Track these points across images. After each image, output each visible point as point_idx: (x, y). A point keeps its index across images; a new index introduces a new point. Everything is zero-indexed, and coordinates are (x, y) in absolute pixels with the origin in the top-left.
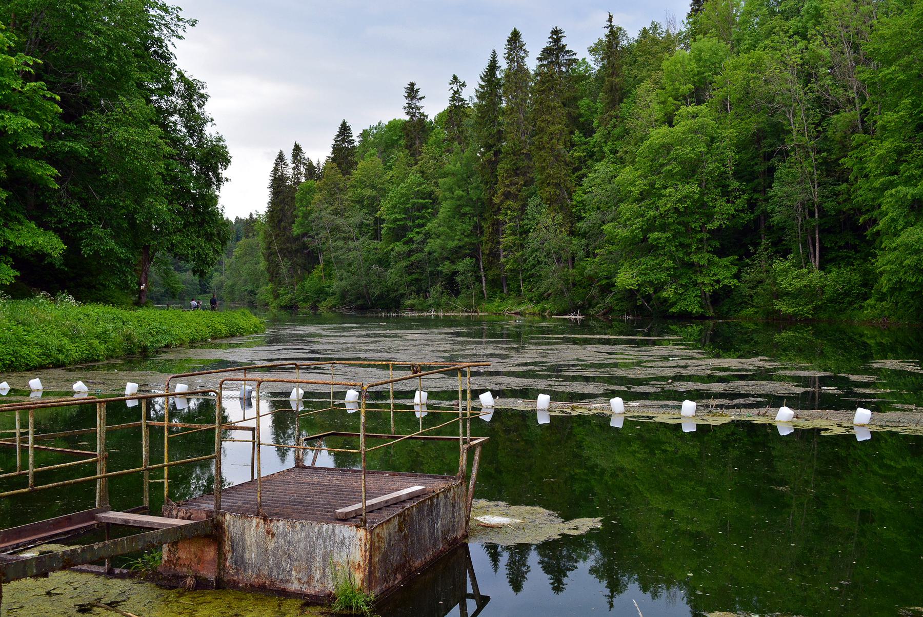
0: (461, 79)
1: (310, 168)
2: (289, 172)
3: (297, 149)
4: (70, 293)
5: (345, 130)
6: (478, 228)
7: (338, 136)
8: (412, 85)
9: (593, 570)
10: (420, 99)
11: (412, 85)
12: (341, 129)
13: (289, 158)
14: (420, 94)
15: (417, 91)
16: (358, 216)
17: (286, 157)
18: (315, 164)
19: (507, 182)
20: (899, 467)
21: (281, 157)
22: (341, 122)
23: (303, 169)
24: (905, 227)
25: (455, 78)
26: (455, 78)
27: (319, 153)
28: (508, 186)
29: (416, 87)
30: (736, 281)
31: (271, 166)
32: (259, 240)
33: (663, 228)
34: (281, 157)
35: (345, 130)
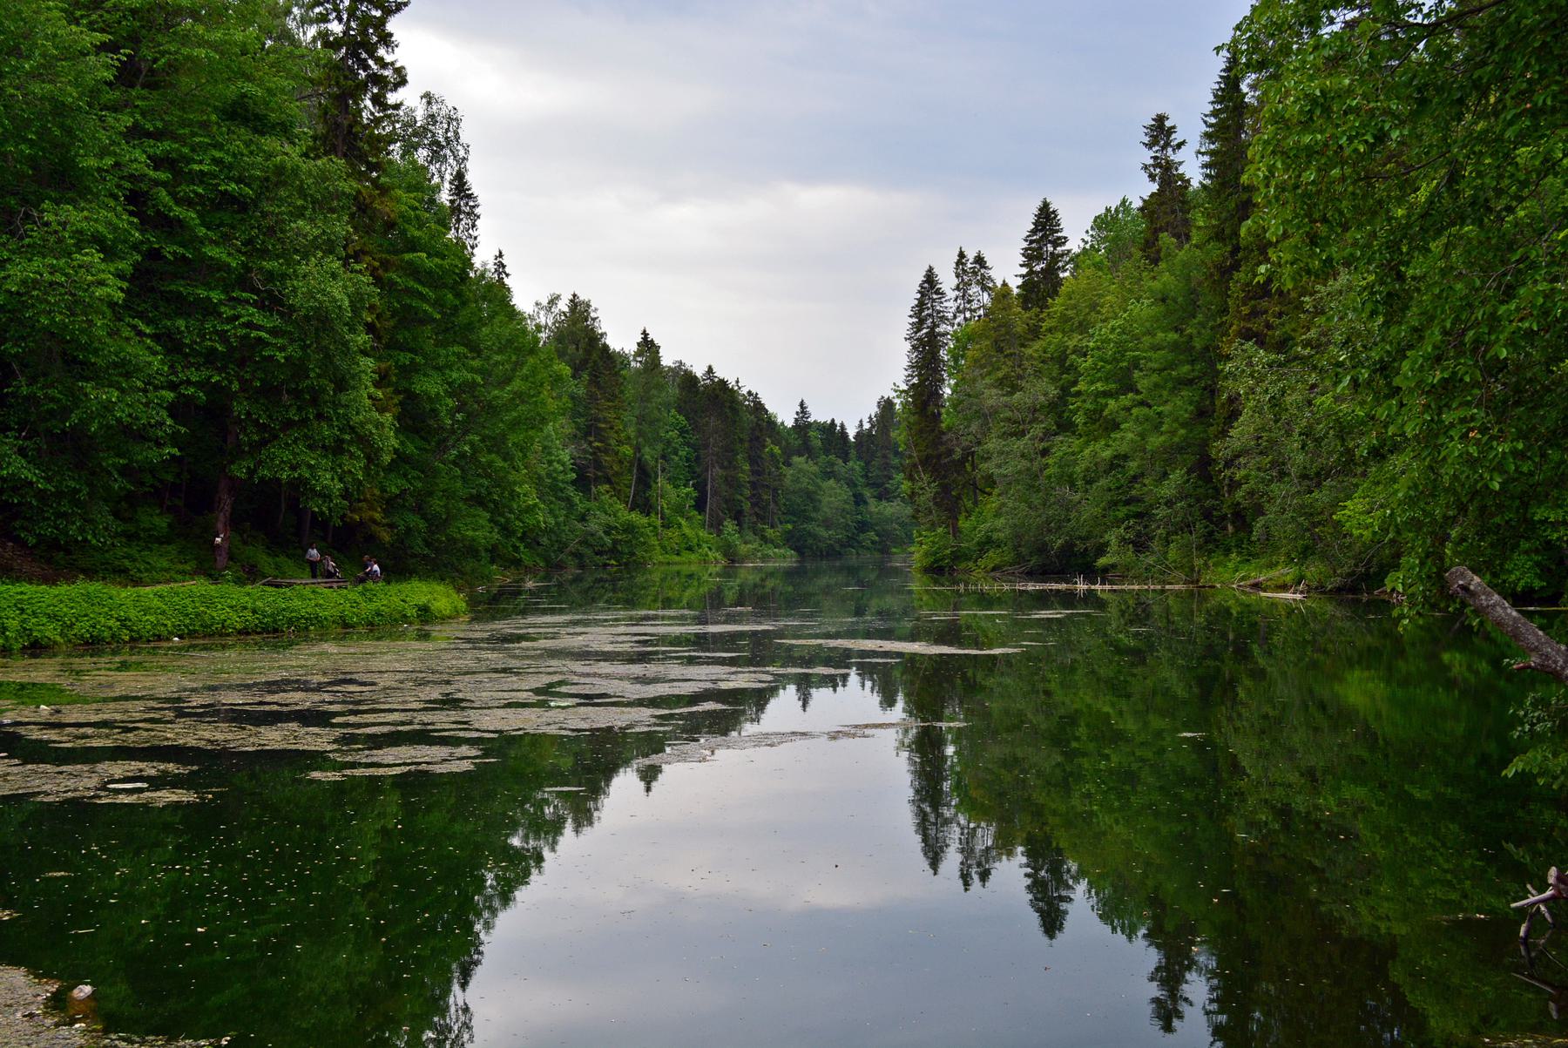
4: (513, 314)
6: (302, 193)
7: (1033, 232)
8: (1160, 119)
9: (1145, 936)
10: (1179, 146)
11: (1160, 119)
12: (1038, 216)
13: (948, 281)
14: (1177, 138)
15: (1172, 130)
16: (1041, 390)
17: (940, 278)
19: (1245, 310)
21: (930, 280)
22: (1039, 204)
28: (1248, 318)
29: (1168, 124)
30: (1130, 395)
34: (930, 280)
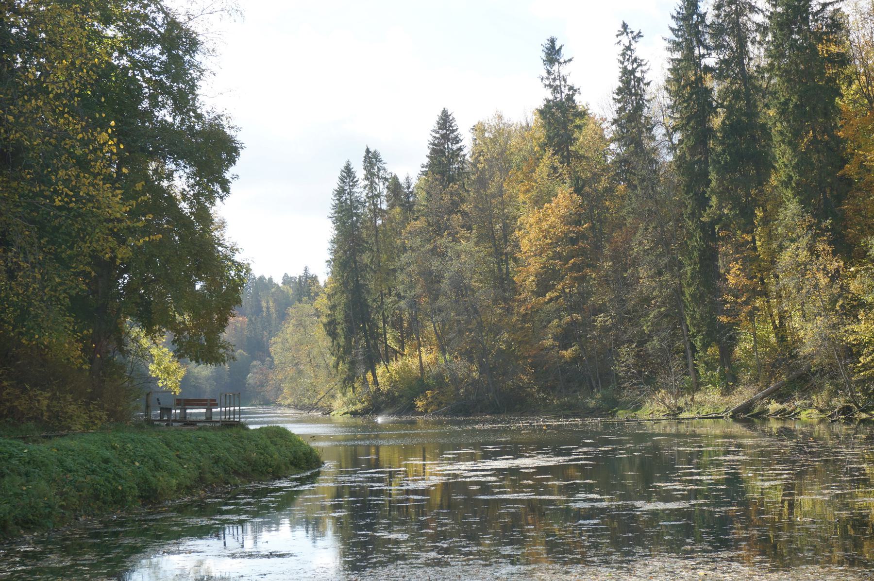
0: (633, 27)
1: (395, 187)
2: (361, 191)
3: (371, 159)
5: (445, 121)
11: (553, 41)
13: (360, 173)
14: (565, 55)
18: (402, 180)
20: (140, 224)
21: (348, 172)
23: (382, 188)
24: (289, 406)
25: (625, 26)
26: (625, 26)
27: (409, 165)
31: (334, 184)
32: (322, 302)
33: (79, 490)
34: (348, 172)
35: (445, 121)
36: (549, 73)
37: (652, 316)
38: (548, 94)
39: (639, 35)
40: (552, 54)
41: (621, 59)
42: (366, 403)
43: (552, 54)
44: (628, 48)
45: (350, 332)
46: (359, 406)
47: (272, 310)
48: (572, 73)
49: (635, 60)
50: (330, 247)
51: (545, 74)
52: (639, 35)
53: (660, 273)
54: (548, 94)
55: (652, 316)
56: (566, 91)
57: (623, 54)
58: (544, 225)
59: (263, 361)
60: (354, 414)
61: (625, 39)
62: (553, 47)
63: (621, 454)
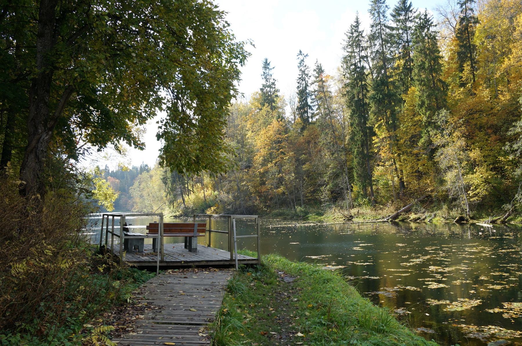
0: (304, 52)
11: (266, 60)
14: (271, 67)
25: (300, 52)
26: (300, 52)
36: (264, 73)
37: (328, 173)
38: (264, 82)
39: (307, 55)
40: (266, 65)
41: (299, 65)
42: (181, 212)
43: (266, 65)
44: (303, 60)
45: (173, 182)
46: (178, 214)
47: (128, 178)
48: (275, 74)
49: (306, 66)
50: (398, 5)
51: (263, 74)
52: (307, 55)
53: (333, 154)
54: (264, 82)
55: (328, 173)
56: (272, 81)
57: (300, 63)
58: (268, 135)
59: (126, 196)
60: (175, 217)
61: (301, 57)
62: (266, 62)
63: (432, 250)
